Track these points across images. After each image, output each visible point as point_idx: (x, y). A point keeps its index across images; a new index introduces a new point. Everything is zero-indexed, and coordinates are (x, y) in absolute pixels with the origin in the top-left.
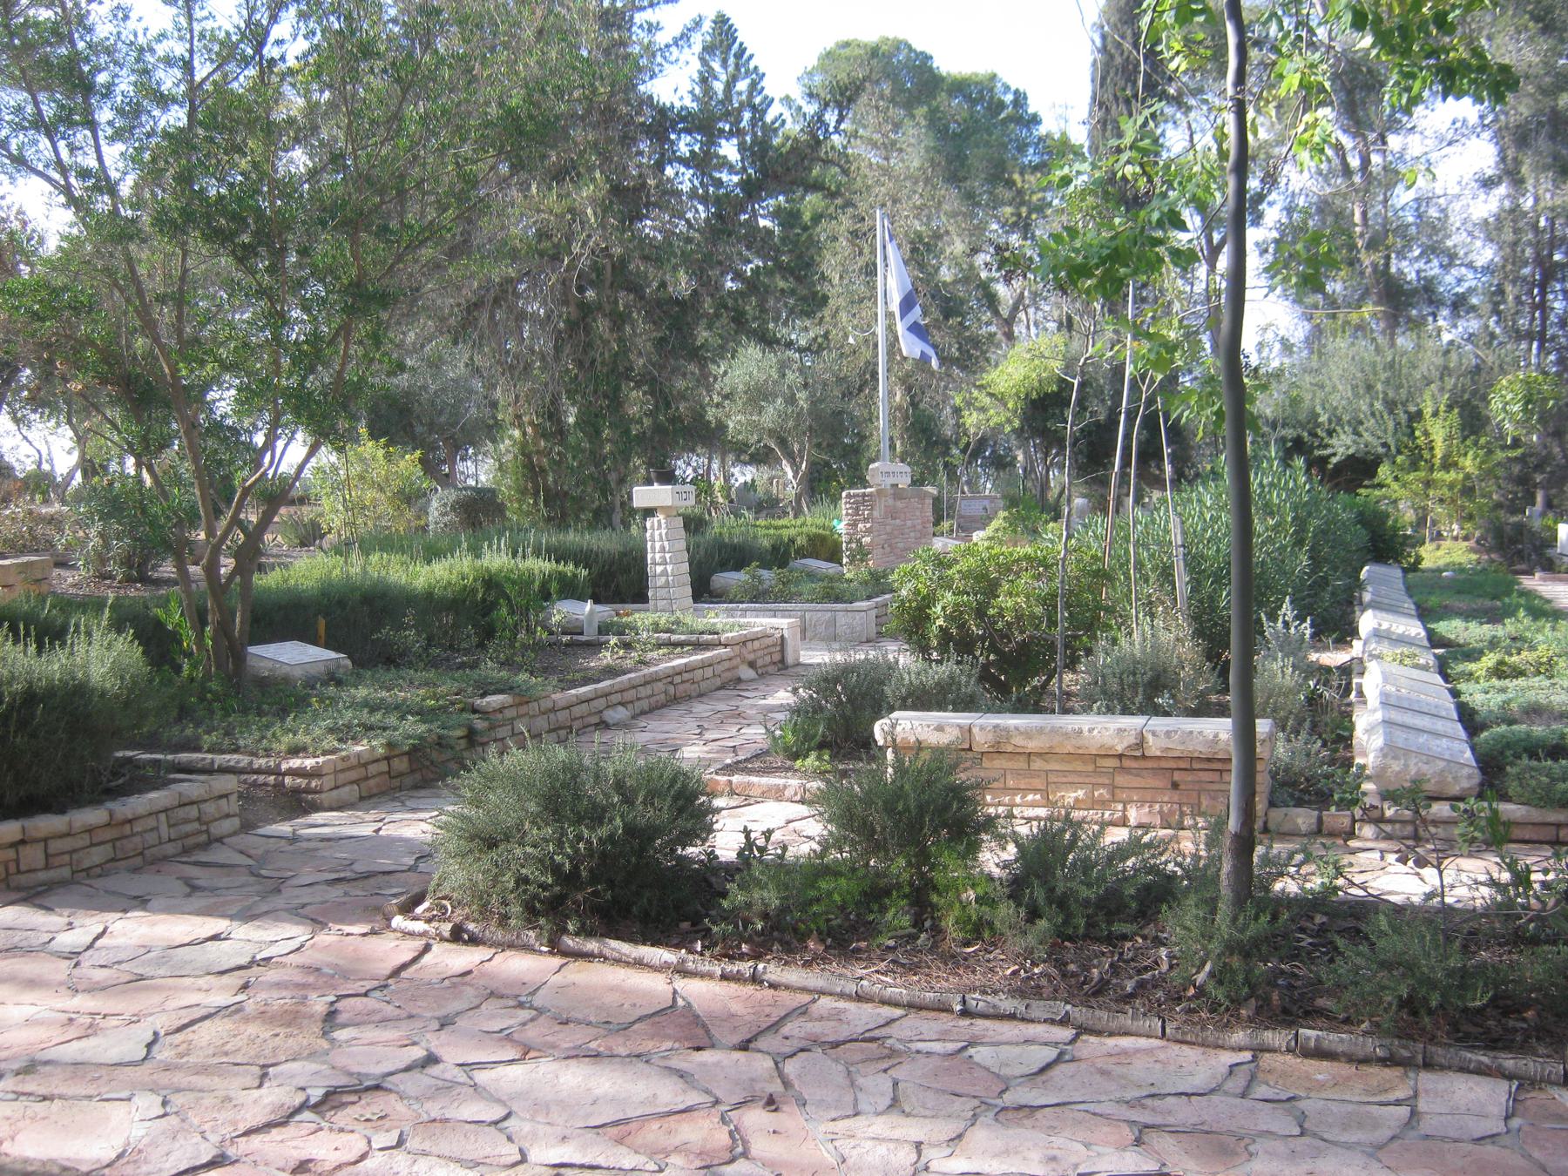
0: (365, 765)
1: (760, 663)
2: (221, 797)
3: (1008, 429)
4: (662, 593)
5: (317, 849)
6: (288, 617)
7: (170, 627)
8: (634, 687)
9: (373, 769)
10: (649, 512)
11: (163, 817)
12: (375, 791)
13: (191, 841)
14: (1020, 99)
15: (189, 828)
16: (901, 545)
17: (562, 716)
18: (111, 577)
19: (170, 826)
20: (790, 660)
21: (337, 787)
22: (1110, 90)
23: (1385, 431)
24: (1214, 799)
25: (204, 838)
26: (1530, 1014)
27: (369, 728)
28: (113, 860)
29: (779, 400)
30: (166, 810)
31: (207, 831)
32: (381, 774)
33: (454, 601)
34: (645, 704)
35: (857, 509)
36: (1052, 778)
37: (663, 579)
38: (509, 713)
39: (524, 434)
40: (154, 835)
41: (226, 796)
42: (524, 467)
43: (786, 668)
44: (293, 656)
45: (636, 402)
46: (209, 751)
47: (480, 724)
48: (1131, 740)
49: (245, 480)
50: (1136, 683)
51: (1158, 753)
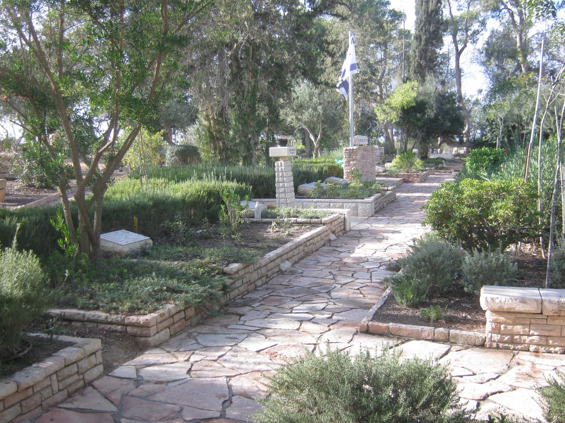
0: (172, 316)
1: (337, 231)
2: (91, 354)
3: (394, 121)
4: (282, 195)
5: (154, 393)
6: (120, 217)
7: (58, 229)
8: (292, 250)
9: (176, 318)
10: (277, 159)
11: (54, 377)
12: (178, 330)
13: (71, 389)
15: (71, 380)
16: (366, 170)
17: (264, 270)
18: (34, 186)
19: (59, 381)
20: (348, 229)
21: (158, 332)
23: (550, 123)
25: (81, 383)
27: (174, 291)
28: (21, 414)
29: (310, 110)
30: (56, 372)
31: (83, 379)
32: (181, 319)
33: (195, 202)
34: (296, 258)
37: (283, 189)
38: (241, 273)
39: (210, 123)
40: (49, 391)
41: (94, 353)
42: (210, 137)
43: (346, 232)
44: (123, 240)
45: (262, 111)
46: (82, 308)
47: (228, 281)
49: (98, 149)
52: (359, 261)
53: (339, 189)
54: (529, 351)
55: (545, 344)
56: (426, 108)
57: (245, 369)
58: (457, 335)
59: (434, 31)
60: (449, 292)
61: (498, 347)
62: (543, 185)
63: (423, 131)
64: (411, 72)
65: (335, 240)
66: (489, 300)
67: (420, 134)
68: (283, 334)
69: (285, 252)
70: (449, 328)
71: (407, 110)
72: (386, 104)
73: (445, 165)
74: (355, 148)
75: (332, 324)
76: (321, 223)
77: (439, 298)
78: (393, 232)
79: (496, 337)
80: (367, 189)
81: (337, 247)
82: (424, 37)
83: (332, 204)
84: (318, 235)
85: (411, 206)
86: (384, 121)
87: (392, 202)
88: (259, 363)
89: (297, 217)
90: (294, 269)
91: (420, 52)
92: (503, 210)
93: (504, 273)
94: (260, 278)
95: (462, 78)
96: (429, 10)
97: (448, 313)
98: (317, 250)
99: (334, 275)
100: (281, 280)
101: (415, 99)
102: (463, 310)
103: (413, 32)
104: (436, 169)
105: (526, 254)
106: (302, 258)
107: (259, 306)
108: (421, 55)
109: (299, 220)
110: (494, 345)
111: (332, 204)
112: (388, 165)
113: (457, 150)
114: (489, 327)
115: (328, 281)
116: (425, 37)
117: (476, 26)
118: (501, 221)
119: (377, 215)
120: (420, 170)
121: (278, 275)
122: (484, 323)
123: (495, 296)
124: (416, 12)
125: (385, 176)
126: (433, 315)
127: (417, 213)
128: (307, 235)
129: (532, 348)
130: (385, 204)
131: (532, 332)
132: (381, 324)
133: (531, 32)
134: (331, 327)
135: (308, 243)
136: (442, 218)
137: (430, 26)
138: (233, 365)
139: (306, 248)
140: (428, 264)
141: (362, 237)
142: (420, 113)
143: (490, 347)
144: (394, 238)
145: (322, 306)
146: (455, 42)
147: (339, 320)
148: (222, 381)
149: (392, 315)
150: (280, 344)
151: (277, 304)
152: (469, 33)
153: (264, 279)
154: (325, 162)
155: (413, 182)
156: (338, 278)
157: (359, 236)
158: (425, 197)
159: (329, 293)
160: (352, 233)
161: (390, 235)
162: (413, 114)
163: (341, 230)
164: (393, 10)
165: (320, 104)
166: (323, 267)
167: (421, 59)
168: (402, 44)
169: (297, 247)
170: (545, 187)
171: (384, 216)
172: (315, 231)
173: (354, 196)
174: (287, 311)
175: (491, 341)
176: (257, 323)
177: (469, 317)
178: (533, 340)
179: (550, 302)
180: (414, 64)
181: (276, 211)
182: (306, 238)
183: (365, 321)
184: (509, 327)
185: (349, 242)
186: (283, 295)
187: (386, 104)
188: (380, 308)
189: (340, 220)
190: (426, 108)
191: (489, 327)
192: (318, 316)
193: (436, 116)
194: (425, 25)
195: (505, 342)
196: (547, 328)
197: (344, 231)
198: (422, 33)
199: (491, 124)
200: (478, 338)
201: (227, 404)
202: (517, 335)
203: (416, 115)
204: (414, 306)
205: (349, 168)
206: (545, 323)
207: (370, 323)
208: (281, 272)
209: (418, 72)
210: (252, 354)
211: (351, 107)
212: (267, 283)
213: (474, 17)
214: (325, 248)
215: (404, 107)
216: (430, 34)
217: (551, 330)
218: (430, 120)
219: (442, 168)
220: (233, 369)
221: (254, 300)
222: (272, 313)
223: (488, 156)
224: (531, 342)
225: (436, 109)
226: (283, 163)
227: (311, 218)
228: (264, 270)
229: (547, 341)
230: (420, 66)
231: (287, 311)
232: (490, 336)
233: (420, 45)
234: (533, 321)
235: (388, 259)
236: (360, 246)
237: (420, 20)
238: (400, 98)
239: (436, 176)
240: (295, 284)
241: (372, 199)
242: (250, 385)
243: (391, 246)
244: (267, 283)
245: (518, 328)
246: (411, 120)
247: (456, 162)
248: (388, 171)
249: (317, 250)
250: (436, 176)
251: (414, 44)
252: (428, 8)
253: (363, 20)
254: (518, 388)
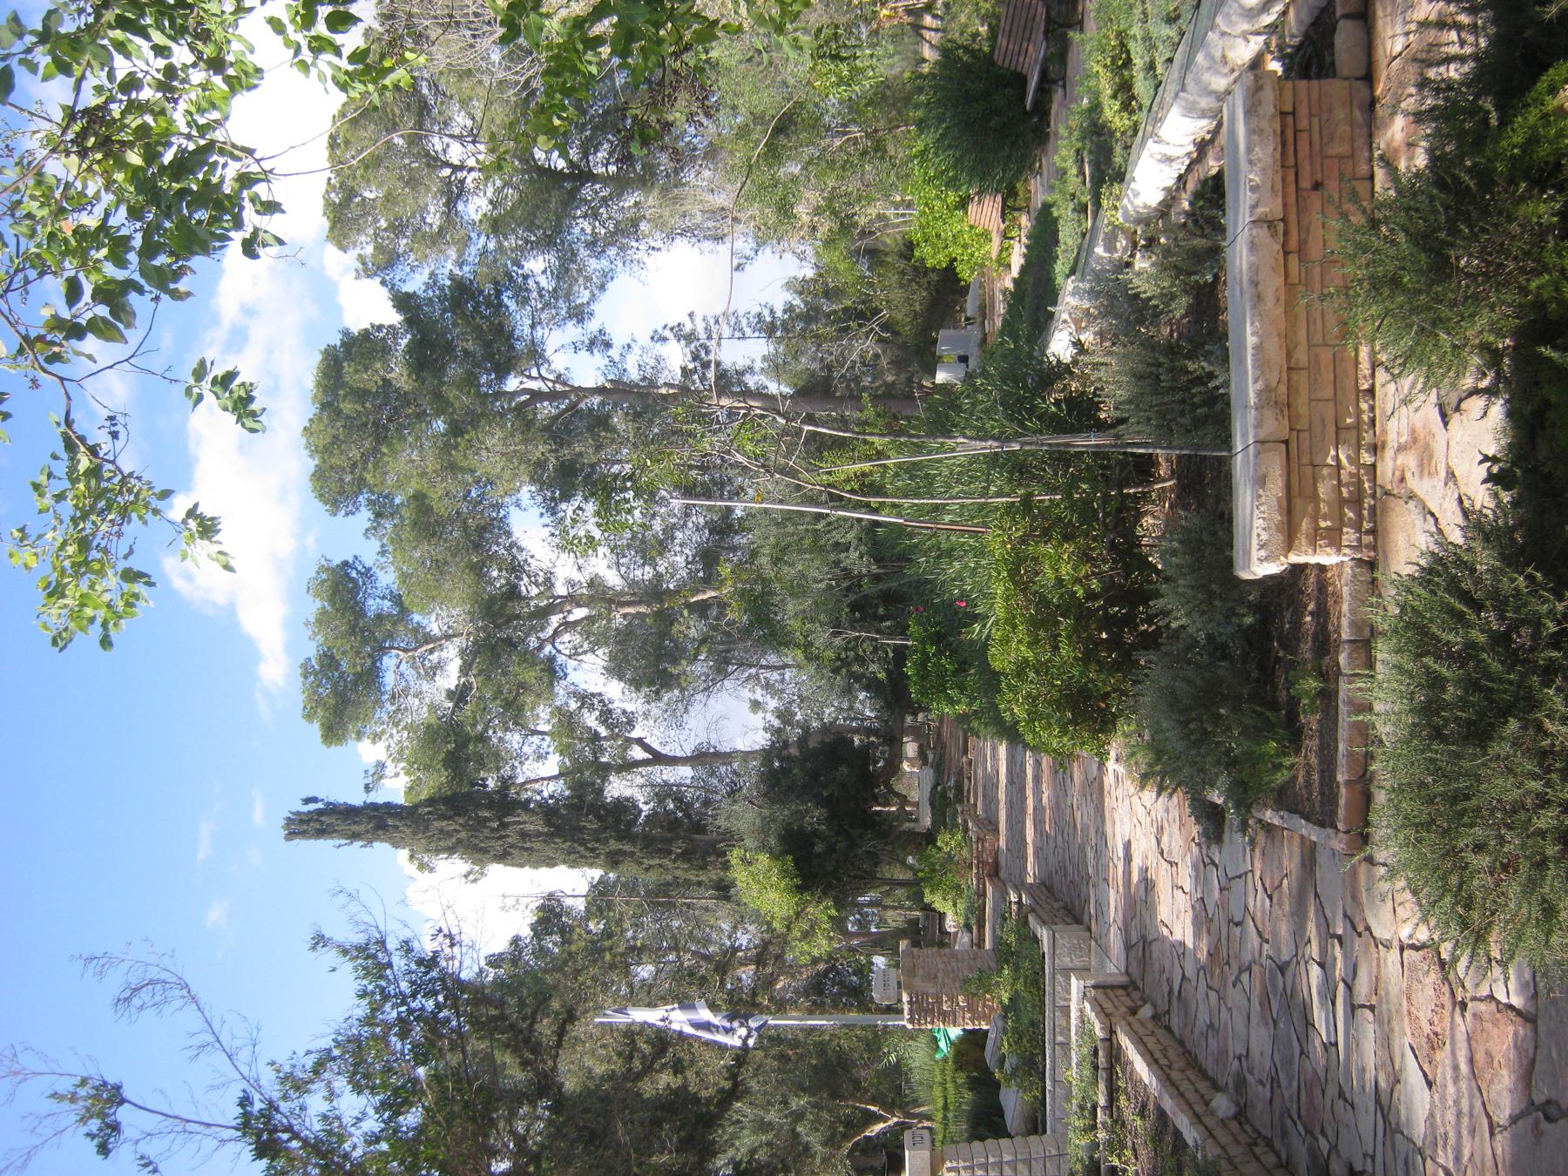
1: (1129, 1003)
3: (833, 912)
20: (1124, 979)
24: (1332, 138)
26: (1468, 163)
34: (1203, 1086)
36: (1318, 338)
48: (1263, 233)
50: (1171, 370)
51: (1279, 200)
52: (1203, 919)
53: (1018, 1020)
54: (1374, 466)
55: (1354, 433)
56: (801, 830)
57: (1471, 1097)
58: (1353, 624)
59: (599, 818)
60: (1262, 668)
61: (1373, 532)
62: (999, 494)
63: (861, 837)
64: (703, 878)
65: (1154, 1005)
66: (1263, 553)
67: (868, 845)
68: (1386, 1042)
69: (1186, 1108)
70: (1338, 643)
71: (803, 877)
72: (788, 928)
73: (952, 783)
74: (905, 998)
75: (1354, 928)
76: (1110, 1040)
77: (1275, 688)
78: (1128, 858)
79: (1349, 536)
80: (1021, 956)
81: (1171, 990)
82: (614, 845)
83: (1059, 1039)
84: (1140, 1042)
85: (1060, 838)
86: (831, 939)
87: (1050, 890)
88: (1456, 1068)
89: (1094, 1107)
90: (1230, 1082)
91: (651, 855)
92: (1059, 565)
93: (1205, 537)
94: (1258, 1159)
95: (722, 749)
97: (1308, 655)
98: (1181, 1043)
99: (1241, 971)
100: (1259, 1107)
101: (775, 856)
102: (1297, 624)
103: (596, 873)
104: (961, 802)
105: (1167, 526)
106: (1204, 1074)
107: (1326, 1137)
108: (659, 851)
109: (1102, 1101)
110: (1367, 539)
111: (1059, 1039)
112: (951, 924)
113: (909, 760)
114: (1328, 558)
115: (1253, 983)
116: (612, 842)
117: (591, 720)
118: (1085, 569)
119: (1086, 917)
120: (964, 837)
121: (1248, 1121)
122: (1322, 568)
123: (1255, 541)
124: (548, 865)
125: (981, 927)
126: (1312, 684)
127: (1078, 815)
128: (1141, 1068)
129: (1367, 458)
130: (1056, 905)
131: (1330, 461)
132: (1342, 802)
133: (613, 579)
134: (1360, 928)
135: (1163, 1061)
136: (1088, 713)
138: (1465, 1133)
139: (1176, 1066)
140: (1194, 714)
141: (1144, 938)
142: (813, 845)
143: (1374, 548)
144: (1143, 849)
145: (1315, 971)
146: (629, 766)
147: (1345, 916)
148: (1502, 1142)
149: (1322, 785)
150: (1408, 1040)
151: (1318, 1092)
152: (603, 731)
153: (1258, 1150)
154: (943, 1084)
155: (997, 853)
156: (1246, 957)
157: (1143, 943)
158: (1035, 809)
159: (1282, 968)
160: (1134, 970)
161: (1137, 863)
163: (1128, 995)
164: (533, 927)
165: (785, 1102)
166: (1223, 1009)
167: (670, 853)
168: (627, 903)
169: (1173, 1084)
170: (1007, 490)
171: (1087, 901)
172: (1125, 1041)
173: (1036, 982)
174: (1334, 1056)
175: (1358, 548)
176: (1367, 1120)
177: (1311, 607)
178: (1348, 457)
179: (1259, 425)
180: (682, 872)
181: (1079, 1167)
182: (1149, 1065)
183: (1338, 843)
184: (1324, 508)
185: (1156, 966)
186: (1295, 1084)
187: (788, 928)
188: (1308, 819)
189: (1101, 997)
190: (801, 828)
191: (1328, 558)
192: (1339, 969)
193: (820, 802)
194: (583, 843)
195: (1360, 516)
196: (1318, 429)
197: (1130, 986)
198: (603, 849)
199: (846, 663)
200: (1354, 576)
201: (1552, 1110)
202: (1340, 492)
203: (819, 856)
204: (1294, 736)
205: (959, 1015)
206: (1306, 434)
207: (1340, 826)
208: (1241, 1115)
209: (704, 859)
210: (1436, 1096)
211: (789, 1022)
212: (1269, 1143)
213: (567, 723)
214: (1175, 1022)
215: (797, 887)
217: (1323, 421)
218: (832, 818)
219: (959, 788)
220: (1473, 1132)
221: (1314, 1153)
222: (1341, 1095)
223: (928, 659)
224: (1355, 460)
225: (804, 802)
226: (948, 1164)
227: (1096, 1068)
228: (1234, 1150)
229: (1348, 428)
230: (686, 856)
231: (1334, 1056)
232: (1347, 551)
234: (1305, 460)
235: (1195, 849)
236: (1165, 931)
237: (569, 853)
238: (773, 895)
239: (980, 798)
240: (1268, 1065)
241: (1044, 934)
242: (1505, 1072)
243: (1162, 853)
244: (1269, 1143)
245: (1323, 490)
246: (830, 869)
247: (942, 756)
248: (967, 918)
249: (1181, 1043)
250: (980, 798)
251: (630, 870)
252: (539, 834)
253: (566, 986)
254: (1448, 467)
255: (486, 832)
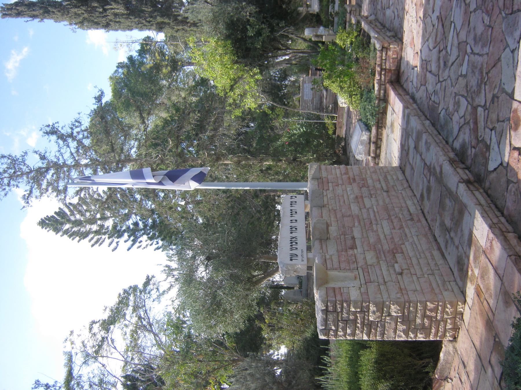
3: (259, 77)
14: (121, 65)
22: (100, 19)
35: (346, 321)
82: (159, 19)
96: (126, 12)
116: (158, 18)
124: (129, 30)
137: (145, 11)
162: (249, 41)
216: (155, 11)
233: (169, 24)
252: (123, 14)
255: (97, 14)
